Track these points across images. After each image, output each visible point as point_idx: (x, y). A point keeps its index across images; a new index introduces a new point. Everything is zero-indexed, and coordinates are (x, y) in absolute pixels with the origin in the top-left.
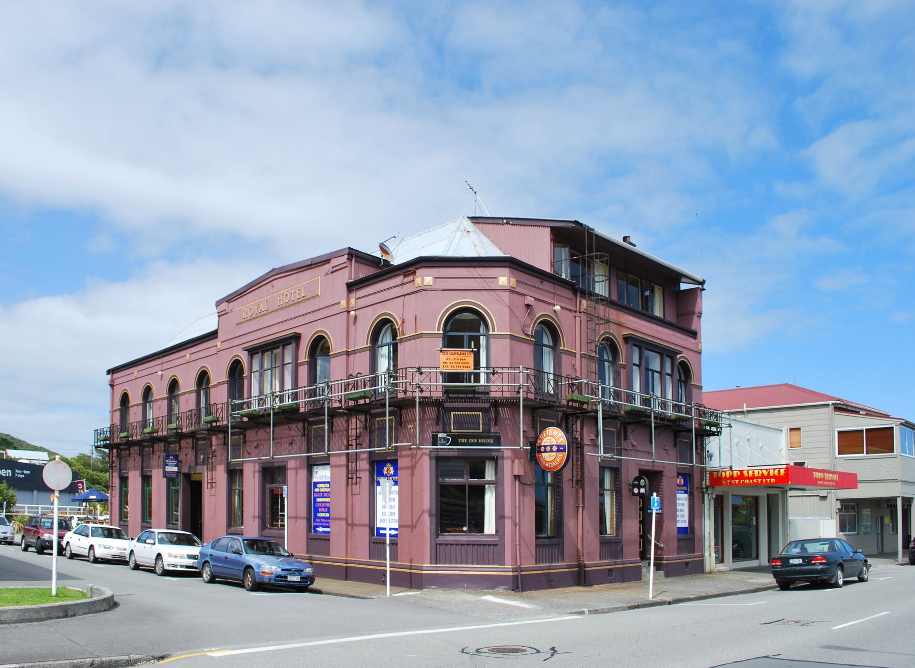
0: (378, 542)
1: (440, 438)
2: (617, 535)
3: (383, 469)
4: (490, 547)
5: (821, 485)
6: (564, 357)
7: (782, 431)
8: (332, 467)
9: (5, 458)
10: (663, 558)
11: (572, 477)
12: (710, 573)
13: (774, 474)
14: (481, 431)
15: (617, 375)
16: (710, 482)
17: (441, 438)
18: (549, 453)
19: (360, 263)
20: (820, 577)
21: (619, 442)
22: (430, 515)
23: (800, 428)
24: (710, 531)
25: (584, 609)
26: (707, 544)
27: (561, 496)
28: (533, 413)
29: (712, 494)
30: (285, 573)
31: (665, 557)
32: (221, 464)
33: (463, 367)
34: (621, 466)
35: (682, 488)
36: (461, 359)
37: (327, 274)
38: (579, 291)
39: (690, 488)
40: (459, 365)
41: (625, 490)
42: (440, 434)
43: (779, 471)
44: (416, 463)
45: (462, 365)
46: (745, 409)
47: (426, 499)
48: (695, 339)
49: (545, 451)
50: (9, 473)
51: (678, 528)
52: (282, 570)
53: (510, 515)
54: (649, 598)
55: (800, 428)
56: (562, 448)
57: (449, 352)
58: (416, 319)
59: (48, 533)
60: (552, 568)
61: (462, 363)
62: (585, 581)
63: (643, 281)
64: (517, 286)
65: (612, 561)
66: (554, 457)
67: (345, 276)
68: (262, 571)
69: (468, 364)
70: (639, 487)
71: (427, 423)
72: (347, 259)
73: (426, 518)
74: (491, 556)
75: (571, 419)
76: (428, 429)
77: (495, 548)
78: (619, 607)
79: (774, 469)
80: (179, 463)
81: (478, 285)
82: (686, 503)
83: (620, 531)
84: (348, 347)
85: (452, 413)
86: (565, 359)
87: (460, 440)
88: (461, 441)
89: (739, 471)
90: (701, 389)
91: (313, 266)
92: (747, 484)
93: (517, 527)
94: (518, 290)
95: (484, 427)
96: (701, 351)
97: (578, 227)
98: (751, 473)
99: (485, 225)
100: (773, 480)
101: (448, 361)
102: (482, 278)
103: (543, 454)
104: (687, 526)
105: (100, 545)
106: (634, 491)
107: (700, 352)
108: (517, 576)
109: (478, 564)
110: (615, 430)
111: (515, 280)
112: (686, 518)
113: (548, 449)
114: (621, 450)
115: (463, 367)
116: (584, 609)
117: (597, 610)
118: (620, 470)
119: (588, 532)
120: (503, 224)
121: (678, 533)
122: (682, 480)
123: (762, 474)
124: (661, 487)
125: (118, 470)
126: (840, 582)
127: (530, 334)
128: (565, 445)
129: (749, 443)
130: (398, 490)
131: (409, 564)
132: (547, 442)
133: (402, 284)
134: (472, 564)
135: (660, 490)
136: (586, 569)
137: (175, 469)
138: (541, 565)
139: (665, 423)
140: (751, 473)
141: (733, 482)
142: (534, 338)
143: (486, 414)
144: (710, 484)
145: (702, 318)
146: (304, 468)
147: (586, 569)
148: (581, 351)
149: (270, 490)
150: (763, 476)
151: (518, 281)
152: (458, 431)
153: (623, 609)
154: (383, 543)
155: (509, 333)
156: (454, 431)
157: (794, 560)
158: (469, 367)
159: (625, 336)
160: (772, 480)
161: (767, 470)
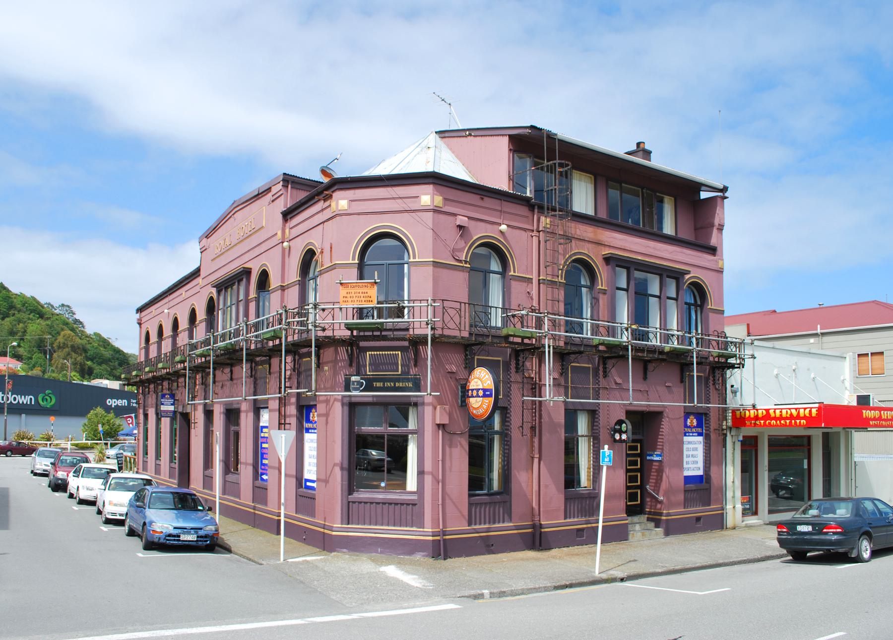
0: (305, 495)
1: (353, 381)
2: (594, 489)
3: (310, 414)
4: (408, 507)
5: (876, 426)
6: (513, 283)
7: (846, 358)
8: (270, 411)
9: (126, 390)
10: (662, 513)
11: (523, 424)
12: (734, 528)
13: (805, 415)
14: (400, 373)
15: (595, 301)
16: (733, 422)
17: (354, 382)
18: (476, 398)
19: (299, 189)
20: (833, 549)
21: (597, 380)
22: (342, 469)
23: (883, 352)
24: (734, 479)
25: (484, 591)
26: (729, 494)
27: (508, 445)
28: (466, 350)
29: (738, 436)
30: (177, 532)
31: (664, 512)
32: (152, 407)
33: (365, 301)
34: (599, 408)
35: (694, 430)
36: (362, 293)
37: (269, 204)
38: (536, 207)
39: (706, 430)
40: (360, 299)
41: (604, 434)
42: (353, 377)
43: (810, 411)
44: (330, 410)
45: (363, 299)
46: (819, 331)
47: (338, 452)
48: (715, 256)
49: (472, 396)
50: (125, 402)
51: (685, 476)
52: (175, 528)
53: (431, 470)
54: (595, 572)
55: (883, 352)
56: (489, 393)
57: (349, 285)
58: (331, 248)
59: (63, 471)
60: (492, 530)
61: (364, 297)
62: (540, 545)
63: (644, 191)
64: (445, 205)
65: (584, 519)
66: (480, 403)
67: (281, 205)
68: (152, 529)
69: (370, 297)
70: (621, 432)
71: (340, 364)
72: (282, 186)
73: (338, 472)
74: (409, 517)
75: (522, 355)
76: (340, 371)
77: (414, 507)
78: (539, 588)
79: (805, 409)
80: (176, 401)
81: (398, 206)
82: (700, 448)
83: (597, 484)
84: (283, 280)
85: (368, 353)
86: (515, 286)
87: (375, 383)
88: (376, 385)
89: (765, 410)
90: (723, 314)
91: (260, 196)
92: (773, 426)
93: (440, 484)
94: (445, 209)
95: (403, 368)
96: (723, 269)
97: (537, 132)
98: (778, 412)
99: (451, 139)
100: (803, 422)
101: (348, 296)
102: (400, 198)
103: (471, 399)
104: (702, 474)
105: (83, 486)
106: (616, 437)
107: (722, 270)
108: (439, 541)
109: (394, 526)
110: (590, 366)
111: (441, 198)
112: (701, 464)
113: (475, 393)
114: (599, 389)
115: (365, 301)
116: (484, 591)
117: (504, 592)
118: (597, 412)
119: (546, 486)
120: (466, 136)
121: (686, 483)
122: (695, 421)
123: (791, 414)
124: (661, 430)
125: (143, 407)
126: (866, 555)
127: (464, 259)
128: (492, 390)
129: (795, 374)
130: (316, 438)
131: (323, 523)
132: (474, 386)
133: (323, 210)
134: (388, 525)
135: (660, 433)
136: (543, 530)
137: (172, 408)
138: (477, 527)
139: (656, 356)
140: (778, 412)
141: (758, 422)
142: (469, 264)
143: (405, 353)
144: (733, 425)
145: (723, 231)
146: (251, 412)
147: (543, 530)
148: (539, 276)
149: (234, 432)
150: (791, 417)
151: (445, 199)
152: (375, 373)
153: (546, 589)
154: (313, 499)
155: (432, 260)
156: (369, 373)
157: (802, 526)
158: (372, 301)
159: (605, 256)
160: (802, 421)
161: (796, 409)
